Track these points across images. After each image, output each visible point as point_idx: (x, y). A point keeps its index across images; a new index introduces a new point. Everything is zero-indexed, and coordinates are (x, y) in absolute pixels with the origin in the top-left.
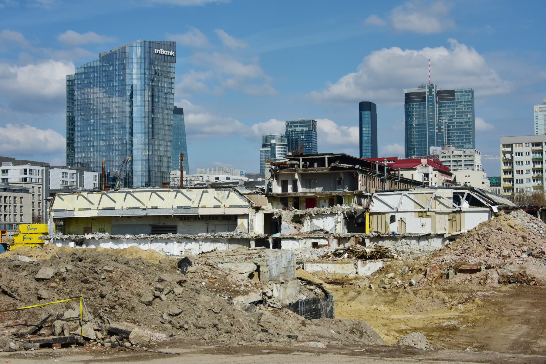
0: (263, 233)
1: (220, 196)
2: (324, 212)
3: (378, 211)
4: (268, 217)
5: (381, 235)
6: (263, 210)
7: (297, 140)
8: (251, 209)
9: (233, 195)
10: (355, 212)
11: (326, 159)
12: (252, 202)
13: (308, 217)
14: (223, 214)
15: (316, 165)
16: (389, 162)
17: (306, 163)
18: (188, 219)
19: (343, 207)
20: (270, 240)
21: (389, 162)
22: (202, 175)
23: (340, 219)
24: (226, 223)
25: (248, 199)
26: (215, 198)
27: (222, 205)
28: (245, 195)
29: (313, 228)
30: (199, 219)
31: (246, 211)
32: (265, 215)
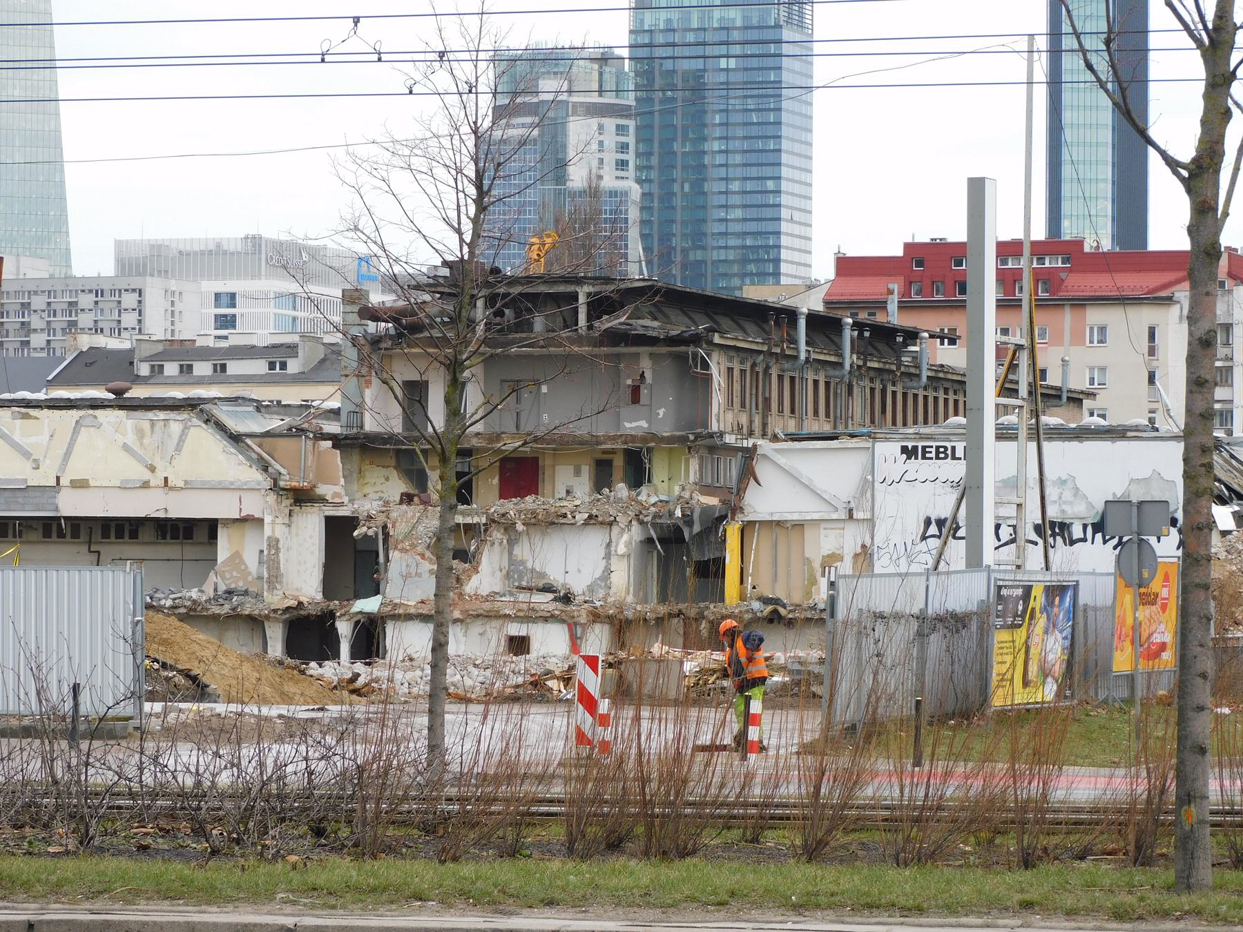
0: (319, 597)
1: (146, 441)
2: (565, 516)
3: (776, 518)
4: (338, 529)
5: (782, 611)
6: (322, 500)
7: (697, 87)
8: (272, 498)
9: (203, 439)
10: (688, 520)
11: (582, 299)
12: (278, 467)
13: (497, 535)
14: (161, 515)
15: (539, 323)
16: (1041, 260)
17: (499, 313)
18: (134, 535)
19: (643, 497)
20: (344, 628)
21: (1041, 260)
22: (136, 283)
23: (628, 544)
24: (171, 550)
25: (261, 458)
26: (126, 448)
27: (157, 480)
28: (249, 441)
29: (520, 579)
30: (61, 535)
31: (253, 505)
32: (331, 522)
